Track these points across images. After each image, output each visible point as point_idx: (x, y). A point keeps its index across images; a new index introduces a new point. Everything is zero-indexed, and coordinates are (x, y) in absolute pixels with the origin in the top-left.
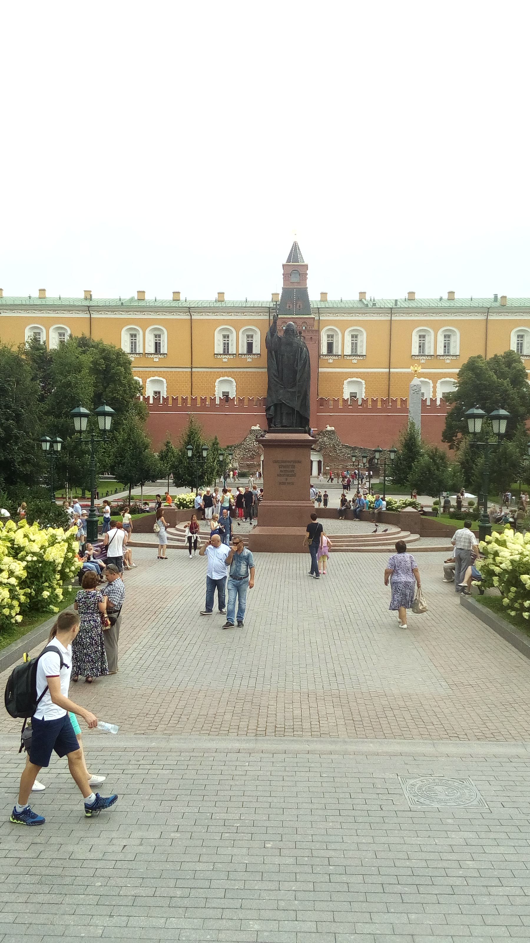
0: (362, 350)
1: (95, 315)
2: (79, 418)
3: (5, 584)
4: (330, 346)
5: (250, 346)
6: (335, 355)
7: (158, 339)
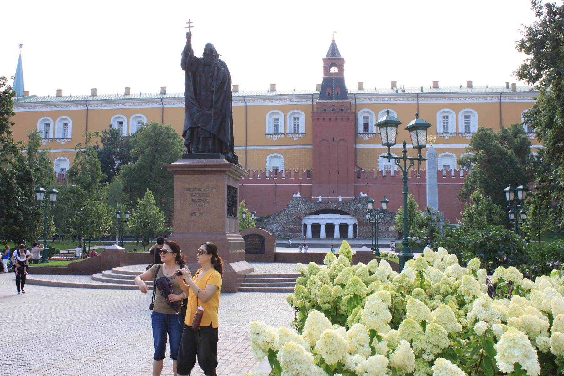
3: (537, 348)
4: (366, 126)
5: (297, 126)
6: (371, 134)
7: (467, 119)
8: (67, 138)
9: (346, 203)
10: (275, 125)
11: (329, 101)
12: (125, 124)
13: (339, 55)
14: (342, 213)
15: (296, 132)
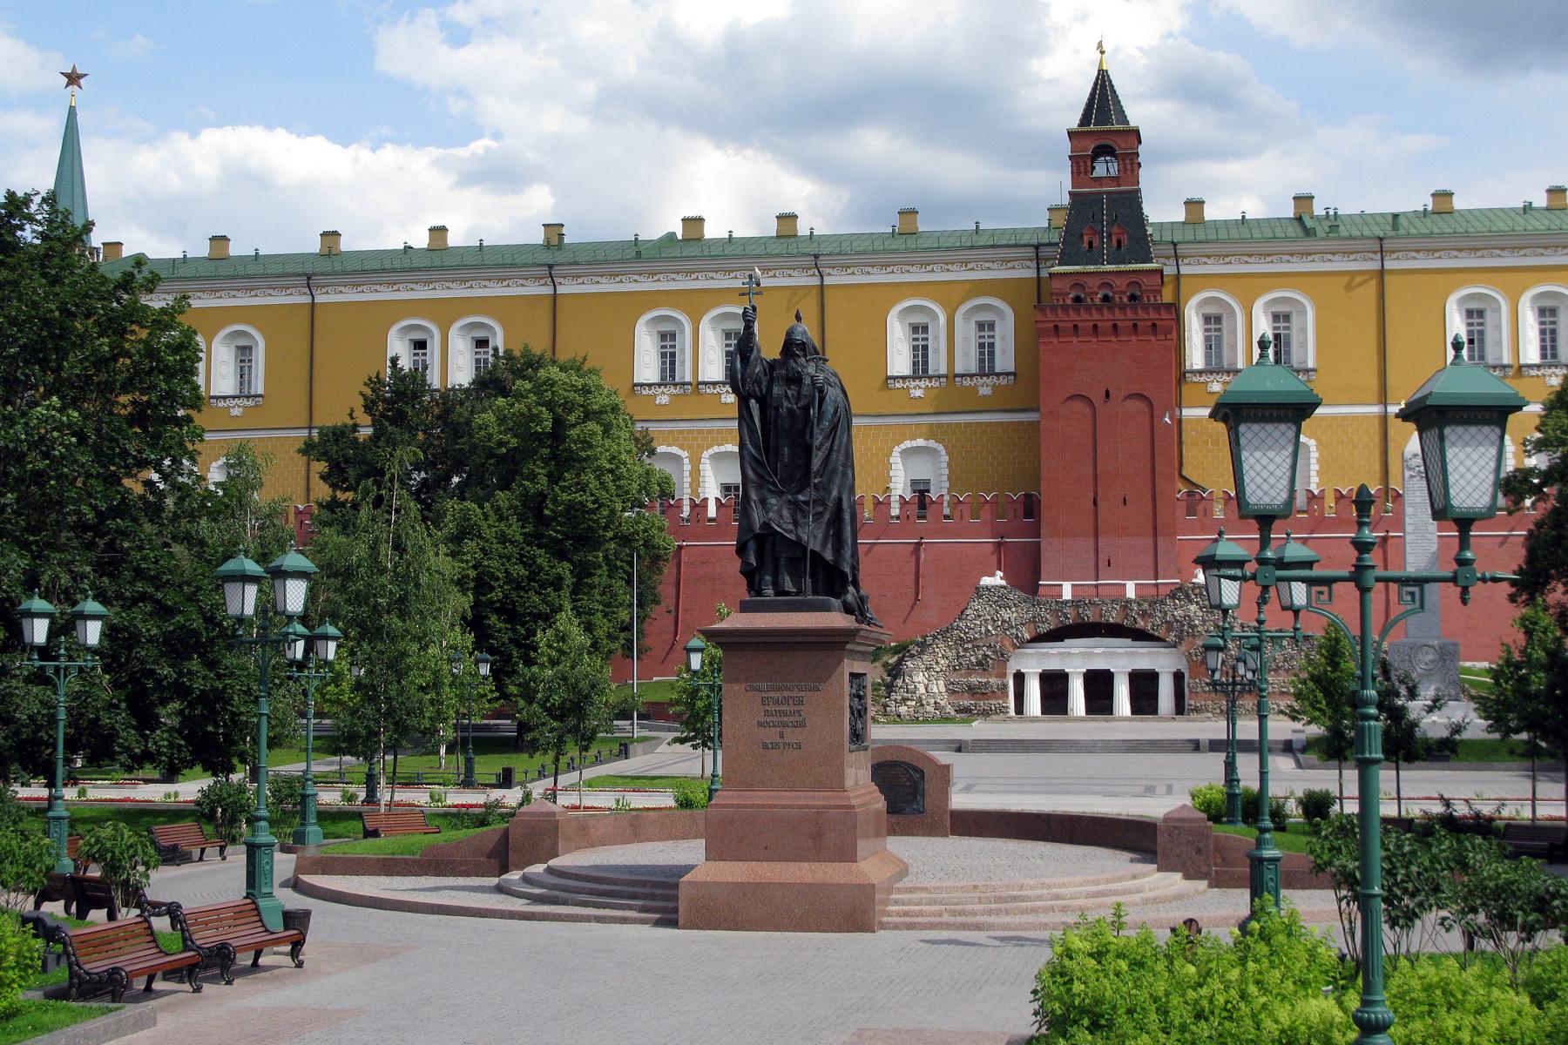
2: (239, 585)
7: (668, 343)
8: (248, 397)
9: (1152, 600)
10: (982, 346)
11: (1092, 268)
12: (434, 346)
14: (1140, 635)
15: (986, 368)
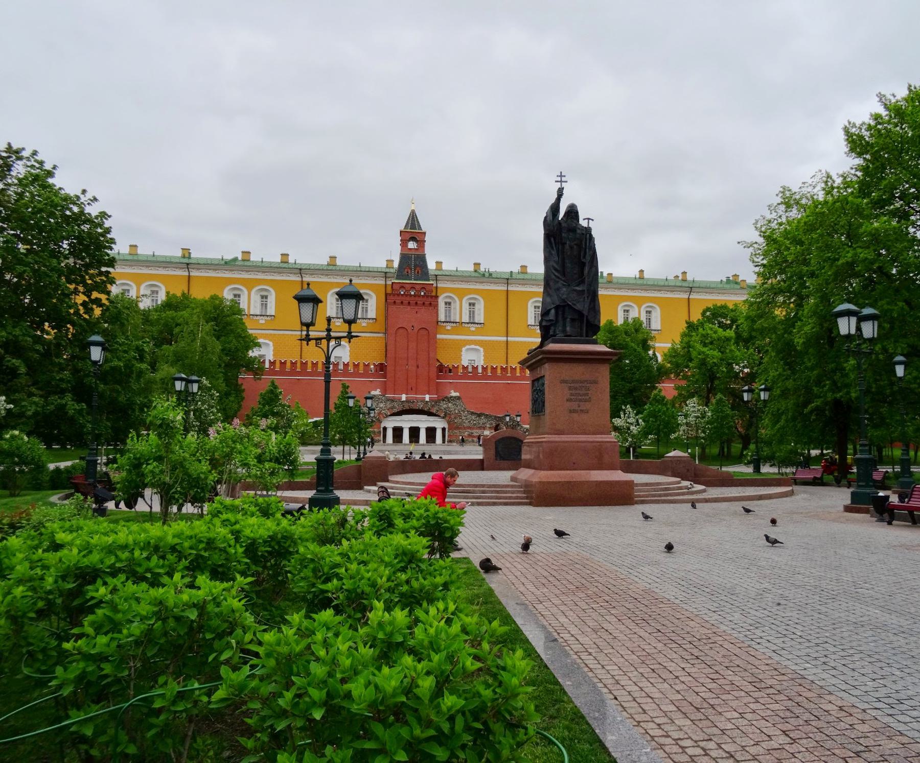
0: (480, 317)
1: (194, 273)
9: (436, 402)
13: (420, 228)
14: (430, 414)
